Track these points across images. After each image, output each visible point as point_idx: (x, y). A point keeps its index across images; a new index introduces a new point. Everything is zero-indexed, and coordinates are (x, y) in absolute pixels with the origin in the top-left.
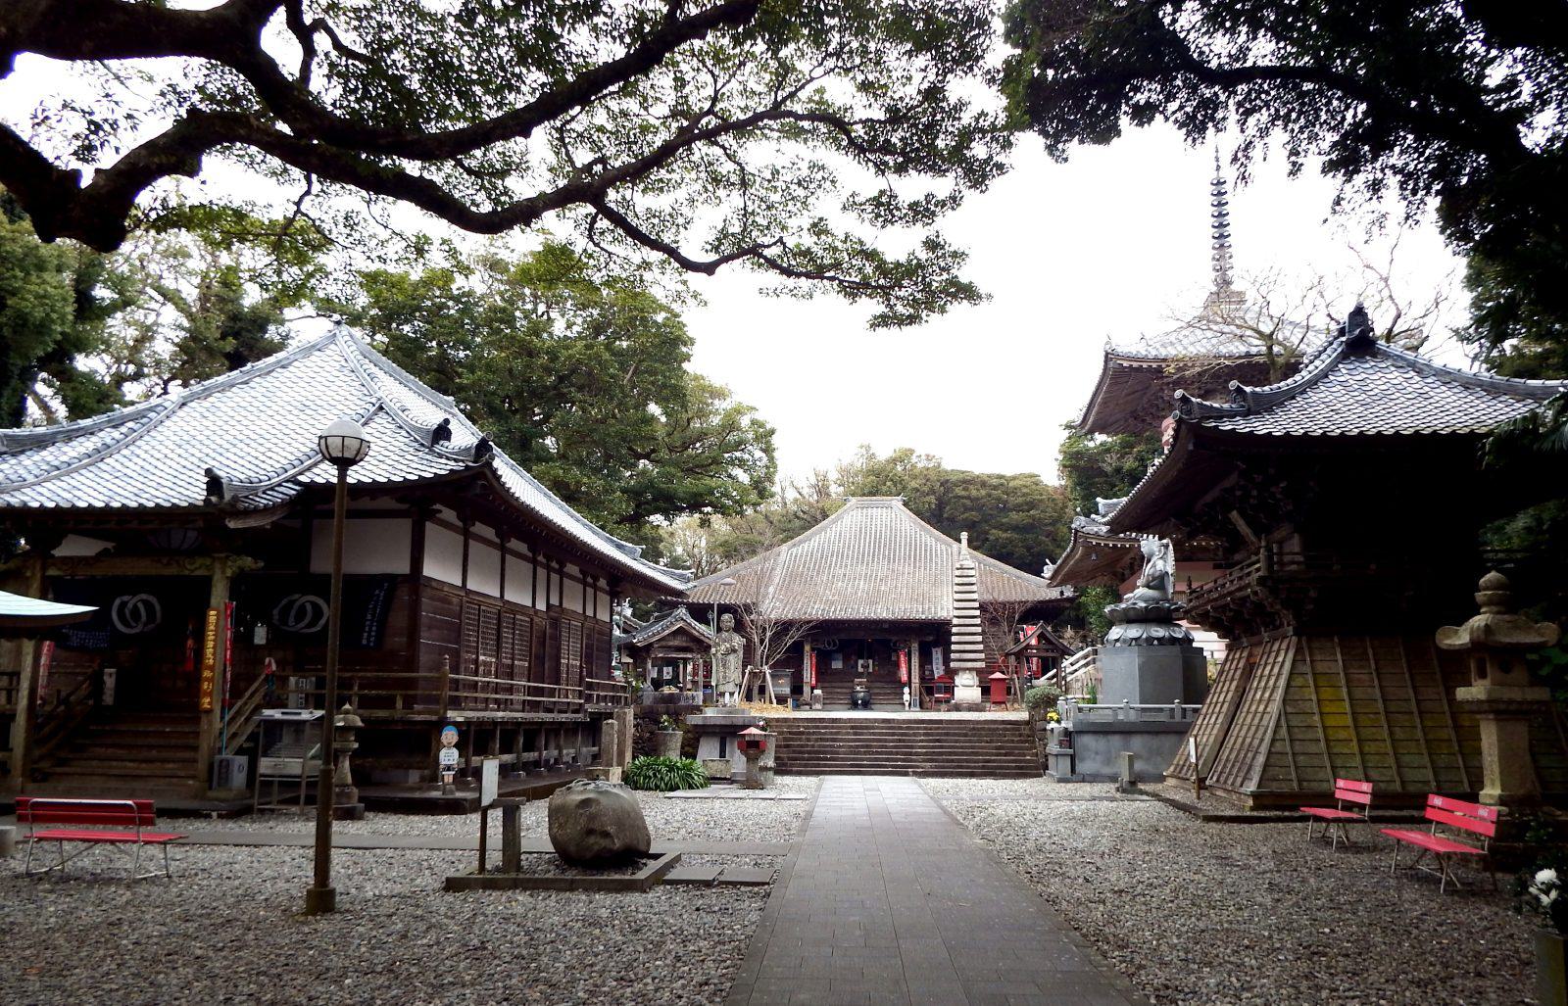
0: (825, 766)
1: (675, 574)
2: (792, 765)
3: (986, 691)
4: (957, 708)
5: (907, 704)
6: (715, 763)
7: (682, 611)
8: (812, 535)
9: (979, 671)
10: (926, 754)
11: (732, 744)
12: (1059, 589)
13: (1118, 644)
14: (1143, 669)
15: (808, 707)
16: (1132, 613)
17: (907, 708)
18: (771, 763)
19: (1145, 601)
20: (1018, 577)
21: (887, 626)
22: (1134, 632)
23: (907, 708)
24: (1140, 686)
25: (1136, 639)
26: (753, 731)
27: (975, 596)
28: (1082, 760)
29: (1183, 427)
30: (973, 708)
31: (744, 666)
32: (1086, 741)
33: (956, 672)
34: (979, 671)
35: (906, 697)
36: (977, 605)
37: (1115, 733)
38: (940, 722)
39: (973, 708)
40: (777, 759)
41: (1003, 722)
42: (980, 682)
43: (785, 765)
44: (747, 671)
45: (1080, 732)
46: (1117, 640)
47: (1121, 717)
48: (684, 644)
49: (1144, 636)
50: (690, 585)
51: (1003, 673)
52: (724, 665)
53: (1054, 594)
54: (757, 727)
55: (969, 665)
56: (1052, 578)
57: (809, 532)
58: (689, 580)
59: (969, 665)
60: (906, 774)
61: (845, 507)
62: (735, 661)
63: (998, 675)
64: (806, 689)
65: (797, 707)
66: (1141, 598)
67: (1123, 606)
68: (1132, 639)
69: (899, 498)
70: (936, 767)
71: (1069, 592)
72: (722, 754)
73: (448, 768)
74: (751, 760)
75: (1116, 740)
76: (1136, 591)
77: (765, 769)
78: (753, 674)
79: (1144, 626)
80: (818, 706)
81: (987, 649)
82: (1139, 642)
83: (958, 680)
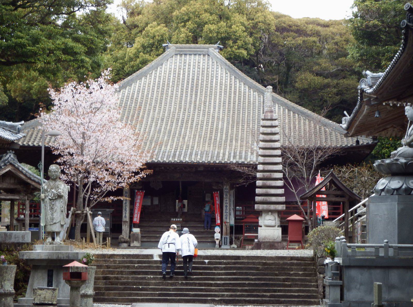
0: (137, 295)
1: (6, 126)
2: (108, 295)
3: (285, 231)
4: (259, 246)
5: (217, 242)
6: (43, 292)
7: (10, 156)
8: (132, 80)
9: (279, 212)
10: (223, 285)
11: (58, 275)
12: (355, 139)
13: (383, 194)
14: (401, 214)
15: (125, 245)
16: (394, 167)
17: (217, 246)
18: (90, 291)
19: (405, 158)
20: (325, 125)
21: (201, 169)
22: (396, 184)
23: (217, 246)
24: (398, 228)
25: (398, 190)
26: (76, 264)
27: (277, 145)
28: (349, 290)
29: (410, 32)
30: (272, 245)
31: (69, 209)
32: (354, 273)
33: (259, 213)
34: (279, 212)
35: (217, 236)
36: (279, 152)
37: (376, 267)
38: (238, 258)
39: (272, 245)
40: (95, 289)
41: (292, 258)
42: (281, 222)
43: (103, 294)
44: (70, 213)
45: (349, 267)
46: (383, 190)
47: (382, 254)
48: (12, 187)
49: (404, 187)
50: (20, 135)
51: (299, 214)
52: (52, 209)
53: (350, 142)
54: (80, 261)
55: (272, 207)
56: (348, 128)
57: (129, 78)
58: (19, 131)
59: (272, 207)
60: (205, 302)
61: (164, 54)
62: (61, 205)
63: (295, 217)
64: (125, 228)
65: (116, 243)
66: (402, 155)
67: (388, 161)
68: (394, 190)
69: (216, 45)
70: (231, 296)
71: (364, 140)
72: (50, 283)
73: (217, 239)
74: (75, 288)
75: (377, 273)
76: (399, 149)
77: (85, 296)
78: (76, 216)
79: (404, 178)
80: (136, 244)
81: (287, 193)
82: (400, 192)
83: (262, 221)
